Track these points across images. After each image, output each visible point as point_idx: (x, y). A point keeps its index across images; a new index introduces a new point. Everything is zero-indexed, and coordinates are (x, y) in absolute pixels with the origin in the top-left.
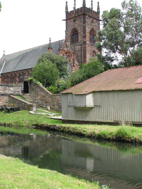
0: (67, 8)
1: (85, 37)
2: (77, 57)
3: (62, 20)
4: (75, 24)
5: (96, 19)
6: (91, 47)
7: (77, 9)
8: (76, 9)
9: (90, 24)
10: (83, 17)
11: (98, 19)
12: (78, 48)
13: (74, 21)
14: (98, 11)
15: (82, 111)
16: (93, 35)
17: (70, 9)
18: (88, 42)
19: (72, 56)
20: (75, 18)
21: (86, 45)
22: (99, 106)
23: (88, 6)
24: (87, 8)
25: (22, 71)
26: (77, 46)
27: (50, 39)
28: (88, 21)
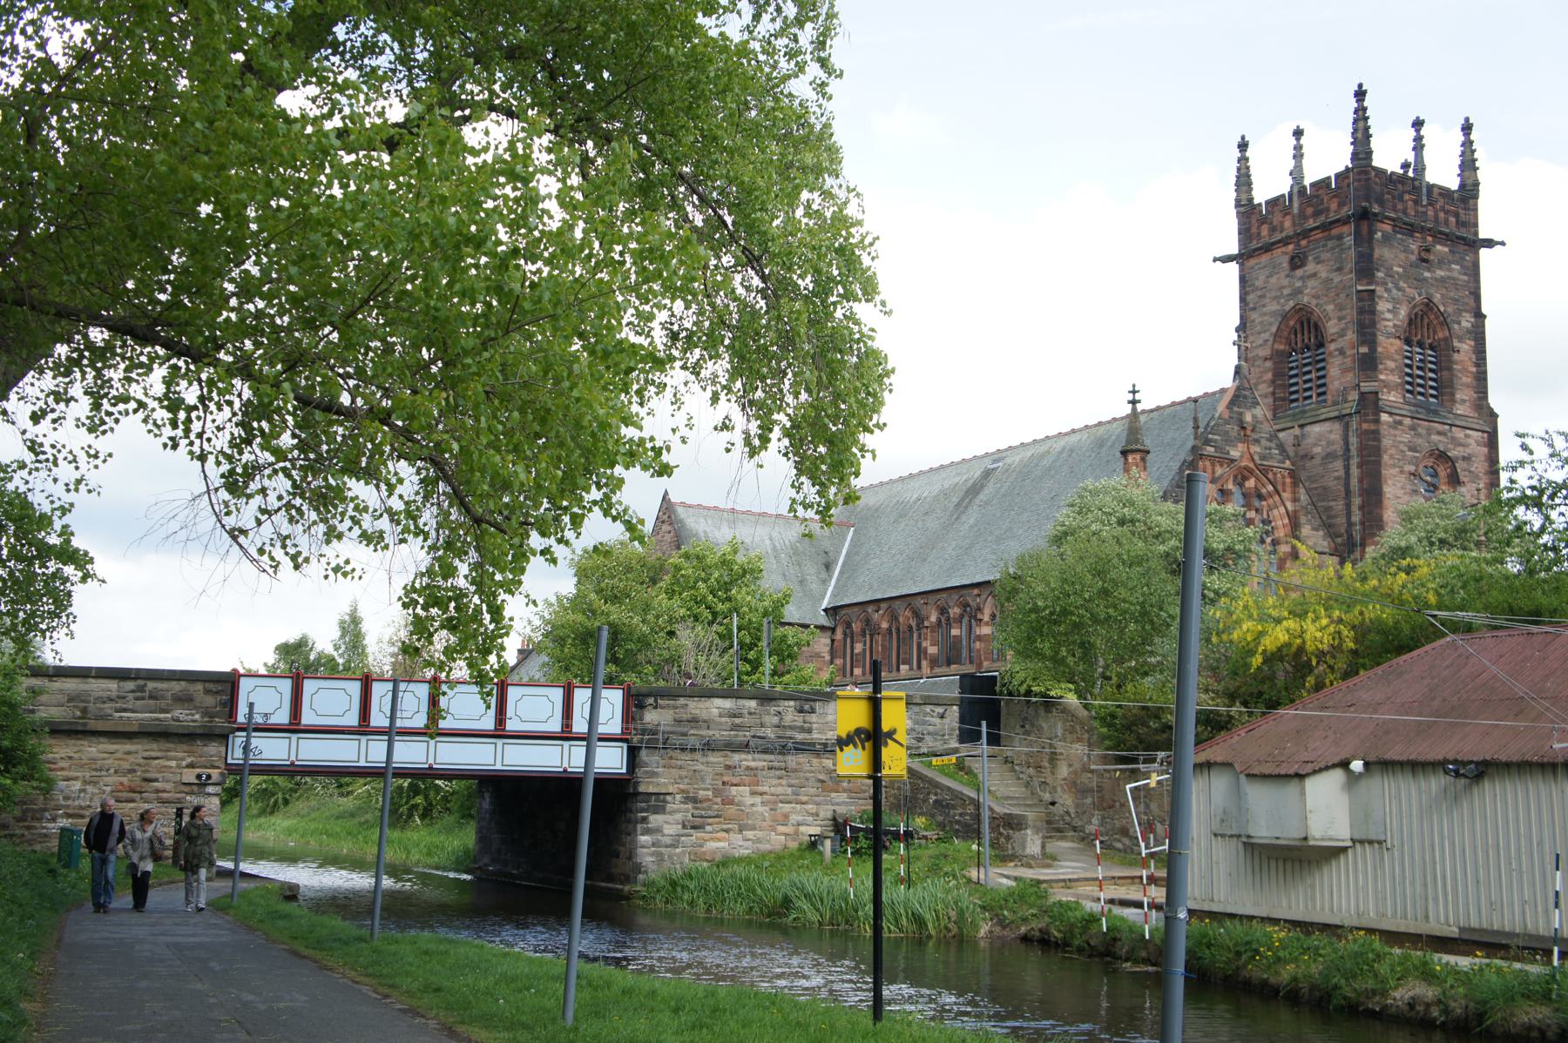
0: (1244, 181)
1: (1369, 364)
2: (1319, 496)
3: (1215, 260)
4: (1299, 284)
5: (1447, 238)
6: (1413, 428)
7: (1312, 185)
8: (1307, 182)
9: (1405, 277)
10: (1357, 233)
11: (1463, 233)
12: (1323, 435)
13: (1297, 262)
14: (1462, 186)
15: (1289, 865)
16: (1432, 348)
17: (1270, 184)
18: (1391, 397)
19: (1285, 495)
20: (1304, 243)
21: (1377, 421)
22: (1379, 843)
23: (1389, 155)
24: (1381, 172)
25: (956, 597)
26: (1317, 428)
27: (1134, 392)
28: (1393, 255)
